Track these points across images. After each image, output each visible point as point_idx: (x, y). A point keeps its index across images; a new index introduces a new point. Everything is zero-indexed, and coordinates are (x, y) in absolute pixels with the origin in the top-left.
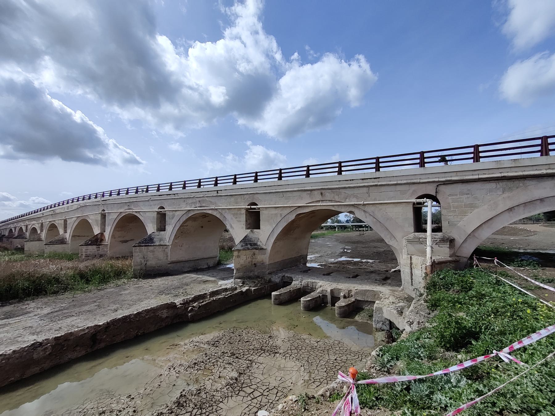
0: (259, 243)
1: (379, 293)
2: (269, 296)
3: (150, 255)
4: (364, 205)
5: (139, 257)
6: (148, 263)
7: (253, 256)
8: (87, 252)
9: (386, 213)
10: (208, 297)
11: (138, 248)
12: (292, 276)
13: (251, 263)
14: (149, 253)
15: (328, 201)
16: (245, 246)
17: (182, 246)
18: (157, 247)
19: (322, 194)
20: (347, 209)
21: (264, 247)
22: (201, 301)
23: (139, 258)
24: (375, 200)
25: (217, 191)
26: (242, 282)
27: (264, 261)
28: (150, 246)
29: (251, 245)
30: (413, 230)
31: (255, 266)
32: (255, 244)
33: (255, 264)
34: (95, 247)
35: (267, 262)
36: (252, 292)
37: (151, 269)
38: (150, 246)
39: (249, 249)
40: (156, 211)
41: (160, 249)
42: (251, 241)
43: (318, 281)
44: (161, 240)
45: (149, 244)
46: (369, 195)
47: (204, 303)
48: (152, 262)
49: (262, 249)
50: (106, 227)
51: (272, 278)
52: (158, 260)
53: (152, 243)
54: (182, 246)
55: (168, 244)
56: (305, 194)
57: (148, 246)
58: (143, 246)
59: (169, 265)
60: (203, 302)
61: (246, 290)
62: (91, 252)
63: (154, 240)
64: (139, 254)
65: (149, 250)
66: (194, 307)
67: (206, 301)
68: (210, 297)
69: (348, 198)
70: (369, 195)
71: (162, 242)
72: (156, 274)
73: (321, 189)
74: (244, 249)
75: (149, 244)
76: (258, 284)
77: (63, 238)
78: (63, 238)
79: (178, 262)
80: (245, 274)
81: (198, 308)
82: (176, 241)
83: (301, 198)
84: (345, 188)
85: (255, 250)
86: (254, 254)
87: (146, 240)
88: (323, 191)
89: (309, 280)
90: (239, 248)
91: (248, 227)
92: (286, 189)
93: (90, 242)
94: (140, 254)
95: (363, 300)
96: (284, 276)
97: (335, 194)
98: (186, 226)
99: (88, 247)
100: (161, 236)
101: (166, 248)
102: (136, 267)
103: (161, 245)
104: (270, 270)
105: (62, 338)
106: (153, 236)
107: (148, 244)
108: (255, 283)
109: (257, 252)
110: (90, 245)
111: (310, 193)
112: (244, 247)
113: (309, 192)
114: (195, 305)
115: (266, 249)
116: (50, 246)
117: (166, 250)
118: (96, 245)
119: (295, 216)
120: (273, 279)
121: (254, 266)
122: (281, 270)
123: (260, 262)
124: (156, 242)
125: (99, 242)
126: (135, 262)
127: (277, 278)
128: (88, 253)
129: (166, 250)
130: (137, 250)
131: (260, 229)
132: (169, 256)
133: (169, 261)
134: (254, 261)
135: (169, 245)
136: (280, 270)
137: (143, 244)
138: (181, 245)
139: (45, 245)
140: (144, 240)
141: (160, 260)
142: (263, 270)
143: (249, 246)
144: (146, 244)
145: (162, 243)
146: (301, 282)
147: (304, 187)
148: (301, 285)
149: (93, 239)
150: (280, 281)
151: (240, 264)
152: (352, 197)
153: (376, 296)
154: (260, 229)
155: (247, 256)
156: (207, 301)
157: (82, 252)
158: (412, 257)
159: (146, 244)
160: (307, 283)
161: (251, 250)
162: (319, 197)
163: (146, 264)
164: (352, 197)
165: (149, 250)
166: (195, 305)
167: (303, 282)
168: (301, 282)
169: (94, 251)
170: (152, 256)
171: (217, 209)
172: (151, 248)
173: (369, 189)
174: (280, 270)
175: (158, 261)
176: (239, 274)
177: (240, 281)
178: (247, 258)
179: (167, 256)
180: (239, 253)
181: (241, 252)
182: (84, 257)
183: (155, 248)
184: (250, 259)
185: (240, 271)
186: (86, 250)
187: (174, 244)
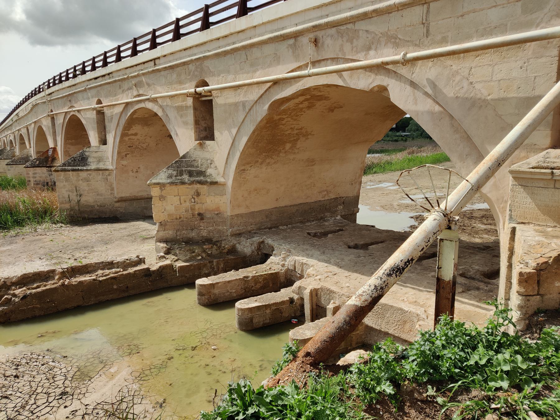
0: (209, 171)
1: (415, 320)
2: (191, 285)
3: (83, 186)
4: (406, 62)
5: (66, 189)
6: (83, 199)
7: (195, 197)
8: (35, 177)
9: (471, 83)
10: (57, 277)
11: (62, 173)
12: (275, 244)
13: (190, 212)
14: (81, 182)
15: (329, 61)
16: (176, 176)
17: (137, 172)
18: (94, 173)
19: (316, 42)
20: (370, 80)
21: (220, 180)
22: (35, 286)
23: (67, 191)
24: (444, 41)
25: (155, 59)
26: (165, 249)
27: (222, 209)
28: (81, 170)
29: (191, 174)
30: (548, 141)
31: (202, 219)
32: (201, 173)
33: (199, 214)
34: (45, 170)
35: (228, 211)
36: (176, 271)
37: (88, 210)
38: (81, 170)
39: (183, 183)
40: (94, 109)
41: (99, 176)
42: (192, 166)
43: (311, 261)
44: (100, 160)
45: (80, 168)
46: (428, 31)
47: (39, 290)
48: (89, 199)
49: (215, 183)
50: (57, 137)
51: (237, 245)
52: (98, 195)
53: (84, 166)
54: (137, 172)
55: (110, 167)
56: (283, 47)
57: (78, 170)
58: (69, 171)
59: (117, 205)
60: (38, 287)
61: (160, 267)
62: (40, 177)
63: (90, 160)
64: (65, 183)
65: (80, 178)
66: (14, 295)
67: (45, 286)
68: (59, 279)
69: (373, 47)
70: (428, 31)
71: (101, 163)
72: (96, 218)
73: (314, 27)
74: (172, 183)
75: (80, 168)
76: (199, 255)
77: (27, 155)
78: (27, 155)
79: (134, 200)
80: (178, 233)
81: (22, 299)
82: (124, 162)
83: (277, 60)
84: (365, 16)
85: (198, 186)
86: (198, 194)
87: (75, 160)
88: (320, 34)
89: (297, 258)
90: (161, 181)
91: (202, 136)
92: (250, 38)
93: (38, 162)
94: (66, 184)
95: (378, 328)
96: (263, 242)
97: (345, 39)
98: (132, 135)
99: (35, 170)
100: (101, 153)
101: (109, 175)
102: (63, 205)
103: (98, 170)
104: (235, 228)
105: (241, 266)
106: (87, 154)
107: (77, 168)
108: (194, 252)
109: (204, 189)
110: (38, 166)
111: (295, 44)
112: (174, 178)
113: (292, 41)
114: (17, 292)
115: (224, 185)
116: (12, 167)
117: (109, 177)
118: (47, 167)
119: (266, 107)
120: (239, 247)
121: (199, 218)
122: (261, 229)
123: (212, 210)
124: (92, 164)
125: (49, 162)
126: (61, 197)
127: (248, 244)
128: (38, 179)
129: (109, 177)
130: (62, 177)
131: (213, 140)
132: (115, 189)
133: (116, 198)
134: (198, 208)
135: (112, 170)
136: (270, 228)
137: (70, 168)
138: (135, 170)
139: (6, 165)
140: (72, 161)
141: (101, 195)
142: (220, 228)
143: (186, 177)
144: (75, 168)
145: (101, 166)
146: (284, 259)
147: (283, 29)
148: (283, 265)
149: (42, 158)
150: (253, 252)
151: (166, 213)
152: (383, 44)
153: (407, 326)
154: (213, 140)
155: (182, 198)
156: (50, 285)
157: (29, 177)
158: (518, 233)
159: (75, 168)
160: (293, 263)
161: (190, 184)
162: (310, 51)
163: (79, 201)
164: (383, 44)
165: (80, 178)
166: (17, 292)
167: (288, 260)
168: (284, 259)
169: (44, 175)
170: (87, 188)
171: (157, 98)
172: (83, 175)
173: (428, 8)
174: (270, 228)
175: (98, 197)
176: (166, 232)
177: (163, 248)
178: (182, 201)
179: (112, 189)
180: (162, 190)
181: (168, 188)
182: (32, 185)
183: (90, 175)
184: (188, 204)
185: (167, 227)
186: (34, 174)
187: (122, 169)
